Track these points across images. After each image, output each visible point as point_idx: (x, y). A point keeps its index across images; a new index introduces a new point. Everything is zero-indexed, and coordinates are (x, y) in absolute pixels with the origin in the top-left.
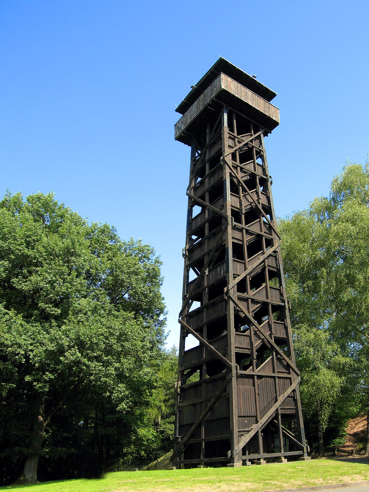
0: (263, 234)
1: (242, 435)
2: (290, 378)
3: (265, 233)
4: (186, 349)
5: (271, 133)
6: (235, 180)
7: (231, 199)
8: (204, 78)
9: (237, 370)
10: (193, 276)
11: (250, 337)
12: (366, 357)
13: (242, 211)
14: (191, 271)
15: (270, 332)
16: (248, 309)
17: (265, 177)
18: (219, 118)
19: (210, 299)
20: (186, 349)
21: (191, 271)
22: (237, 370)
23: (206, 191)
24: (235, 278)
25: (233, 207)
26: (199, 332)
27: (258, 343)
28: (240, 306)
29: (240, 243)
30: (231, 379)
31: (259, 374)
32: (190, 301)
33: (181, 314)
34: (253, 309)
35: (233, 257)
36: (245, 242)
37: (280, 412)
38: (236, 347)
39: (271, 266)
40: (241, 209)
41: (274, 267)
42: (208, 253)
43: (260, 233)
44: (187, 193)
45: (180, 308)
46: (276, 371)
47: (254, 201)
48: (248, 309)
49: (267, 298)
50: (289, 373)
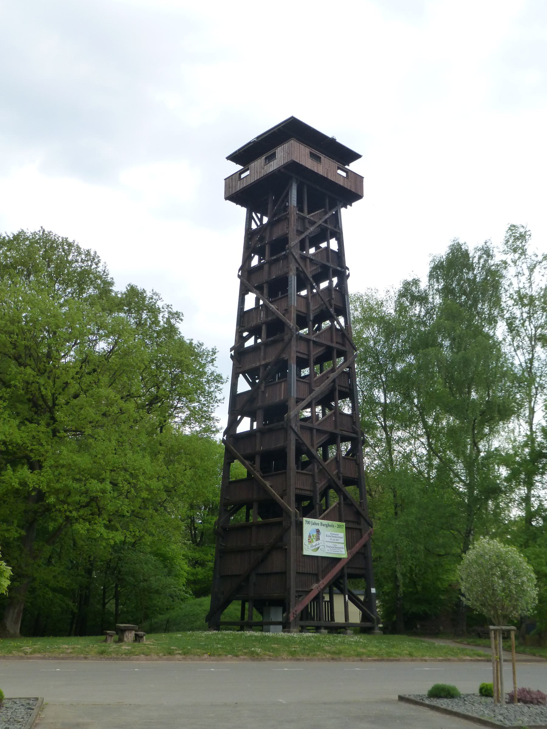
0: (334, 345)
1: (300, 596)
2: (360, 530)
3: (337, 343)
4: (246, 309)
5: (351, 205)
6: (302, 275)
7: (297, 386)
8: (264, 136)
9: (296, 517)
10: (250, 301)
11: (313, 476)
12: (419, 316)
13: (309, 317)
14: (241, 378)
15: (336, 471)
16: (312, 441)
17: (339, 268)
18: (284, 193)
19: (272, 254)
20: (246, 309)
21: (241, 378)
22: (296, 517)
23: (265, 283)
24: (297, 402)
25: (299, 311)
26: (259, 289)
27: (323, 483)
28: (303, 438)
29: (305, 357)
30: (290, 527)
31: (320, 428)
32: (239, 417)
33: (241, 269)
34: (318, 441)
35: (297, 468)
36: (312, 356)
37: (346, 571)
38: (297, 352)
39: (342, 387)
40: (308, 314)
41: (346, 388)
42: (266, 366)
43: (334, 431)
44: (238, 275)
45: (240, 264)
46: (335, 340)
47: (324, 303)
48: (312, 441)
49: (328, 261)
50: (359, 523)
